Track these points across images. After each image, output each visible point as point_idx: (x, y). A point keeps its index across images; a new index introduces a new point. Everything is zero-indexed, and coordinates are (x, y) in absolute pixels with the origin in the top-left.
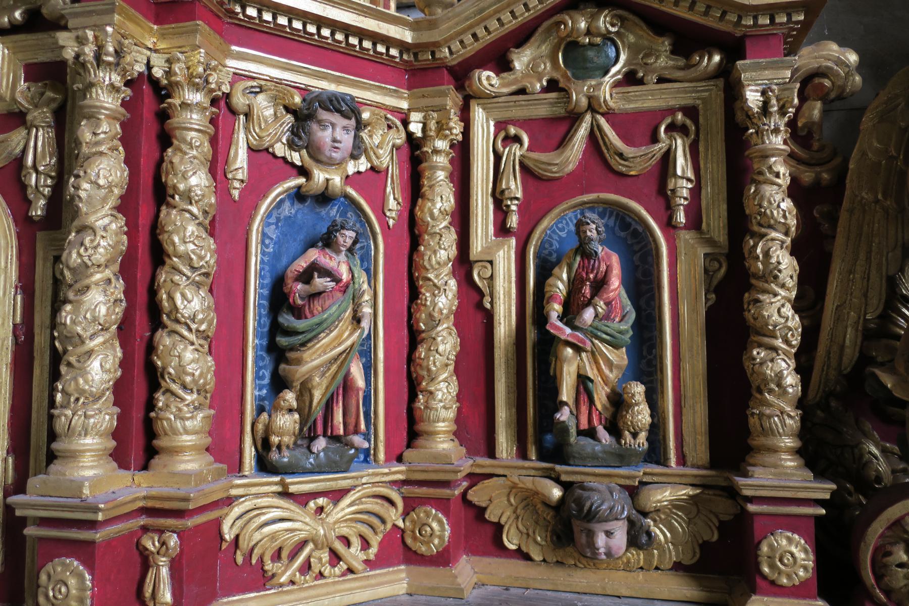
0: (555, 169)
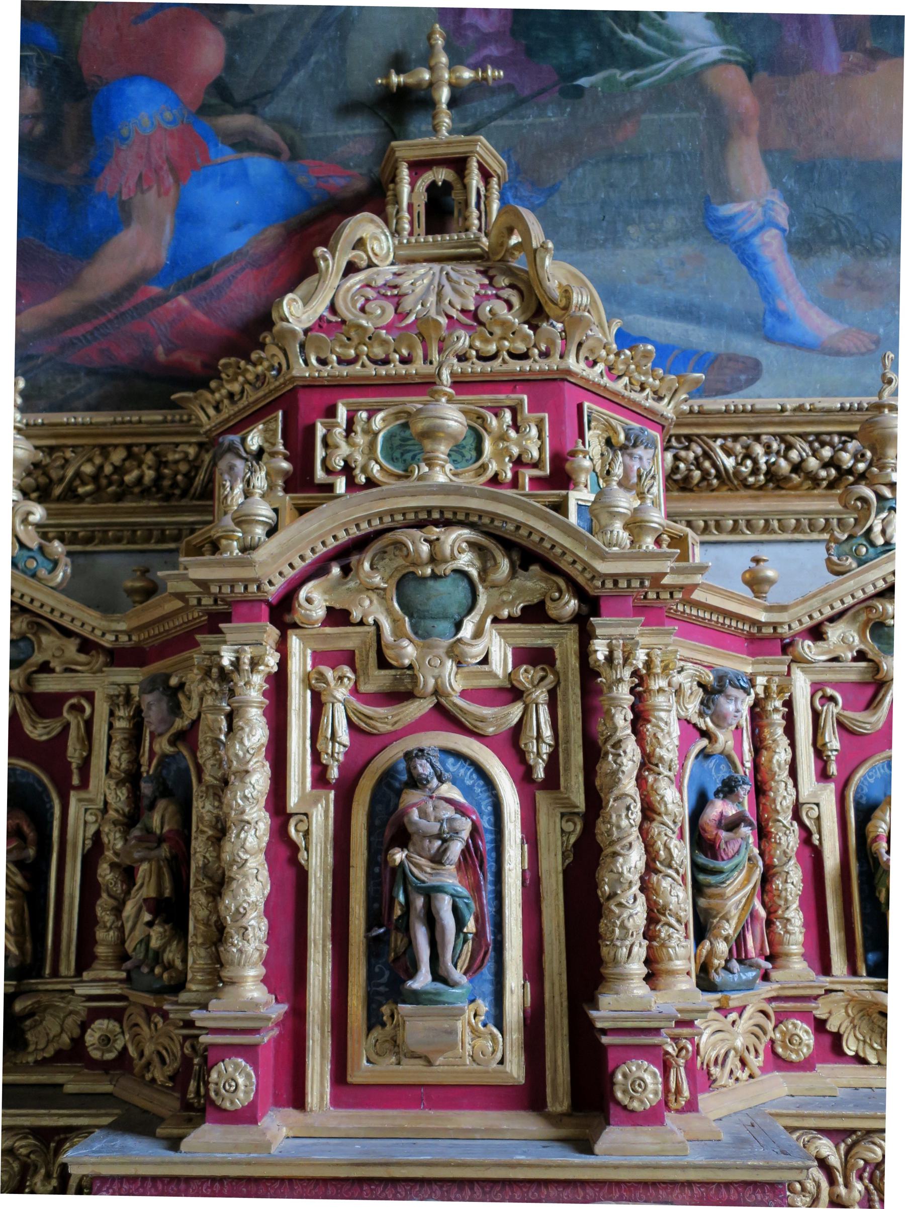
0: (868, 727)
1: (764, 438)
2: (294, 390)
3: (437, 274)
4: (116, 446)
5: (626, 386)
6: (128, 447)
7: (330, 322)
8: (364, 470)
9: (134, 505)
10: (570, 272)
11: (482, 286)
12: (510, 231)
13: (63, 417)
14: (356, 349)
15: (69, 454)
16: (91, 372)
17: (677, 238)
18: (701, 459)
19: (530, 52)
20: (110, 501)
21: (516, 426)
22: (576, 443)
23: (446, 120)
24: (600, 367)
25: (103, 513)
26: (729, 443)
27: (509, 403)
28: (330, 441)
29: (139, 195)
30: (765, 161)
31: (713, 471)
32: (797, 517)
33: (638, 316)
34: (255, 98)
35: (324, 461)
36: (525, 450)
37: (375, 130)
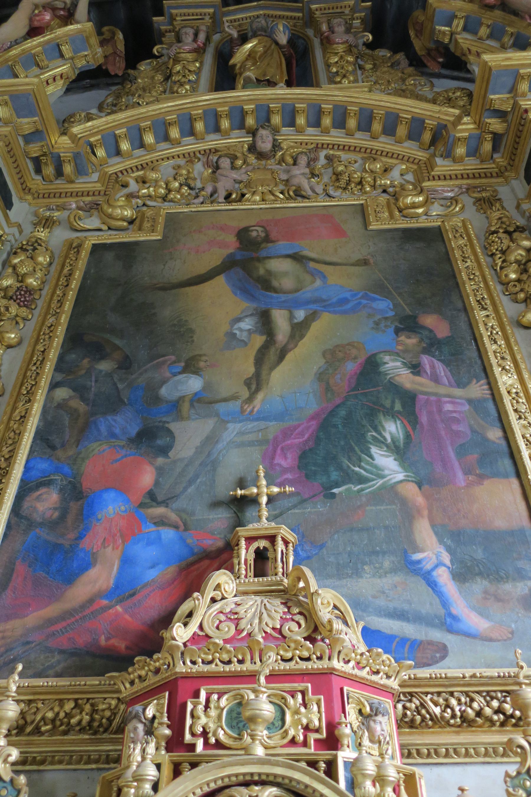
1: (456, 694)
2: (176, 679)
3: (259, 605)
4: (69, 700)
5: (368, 672)
6: (76, 700)
7: (199, 635)
8: (215, 734)
9: (74, 737)
10: (333, 594)
11: (284, 613)
12: (299, 579)
13: (40, 682)
14: (213, 655)
15: (40, 705)
16: (62, 652)
17: (391, 573)
18: (420, 708)
19: (307, 476)
20: (60, 735)
21: (305, 705)
22: (341, 716)
23: (265, 513)
24: (352, 664)
25: (55, 743)
26: (435, 698)
27: (300, 688)
28: (195, 714)
29: (102, 549)
30: (434, 530)
31: (428, 716)
32: (486, 746)
33: (374, 618)
34: (167, 500)
35: (191, 727)
36: (310, 721)
37: (228, 515)
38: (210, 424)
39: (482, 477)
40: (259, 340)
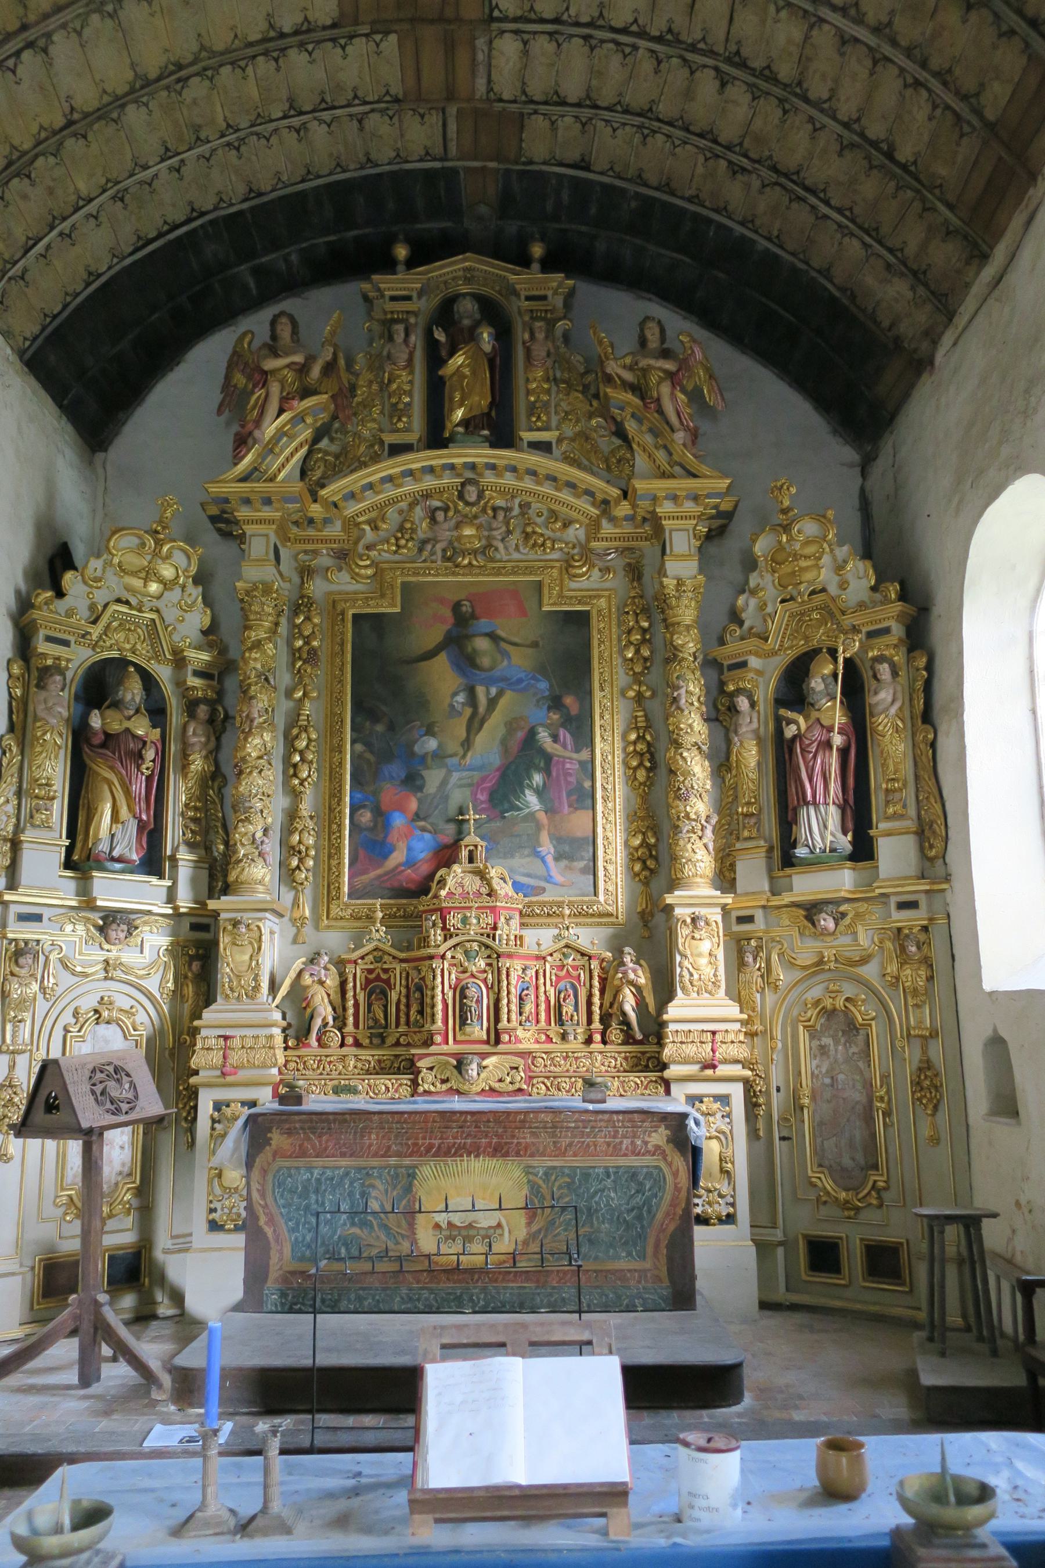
38: (444, 771)
39: (576, 809)
40: (468, 711)
